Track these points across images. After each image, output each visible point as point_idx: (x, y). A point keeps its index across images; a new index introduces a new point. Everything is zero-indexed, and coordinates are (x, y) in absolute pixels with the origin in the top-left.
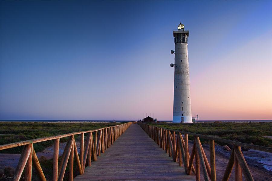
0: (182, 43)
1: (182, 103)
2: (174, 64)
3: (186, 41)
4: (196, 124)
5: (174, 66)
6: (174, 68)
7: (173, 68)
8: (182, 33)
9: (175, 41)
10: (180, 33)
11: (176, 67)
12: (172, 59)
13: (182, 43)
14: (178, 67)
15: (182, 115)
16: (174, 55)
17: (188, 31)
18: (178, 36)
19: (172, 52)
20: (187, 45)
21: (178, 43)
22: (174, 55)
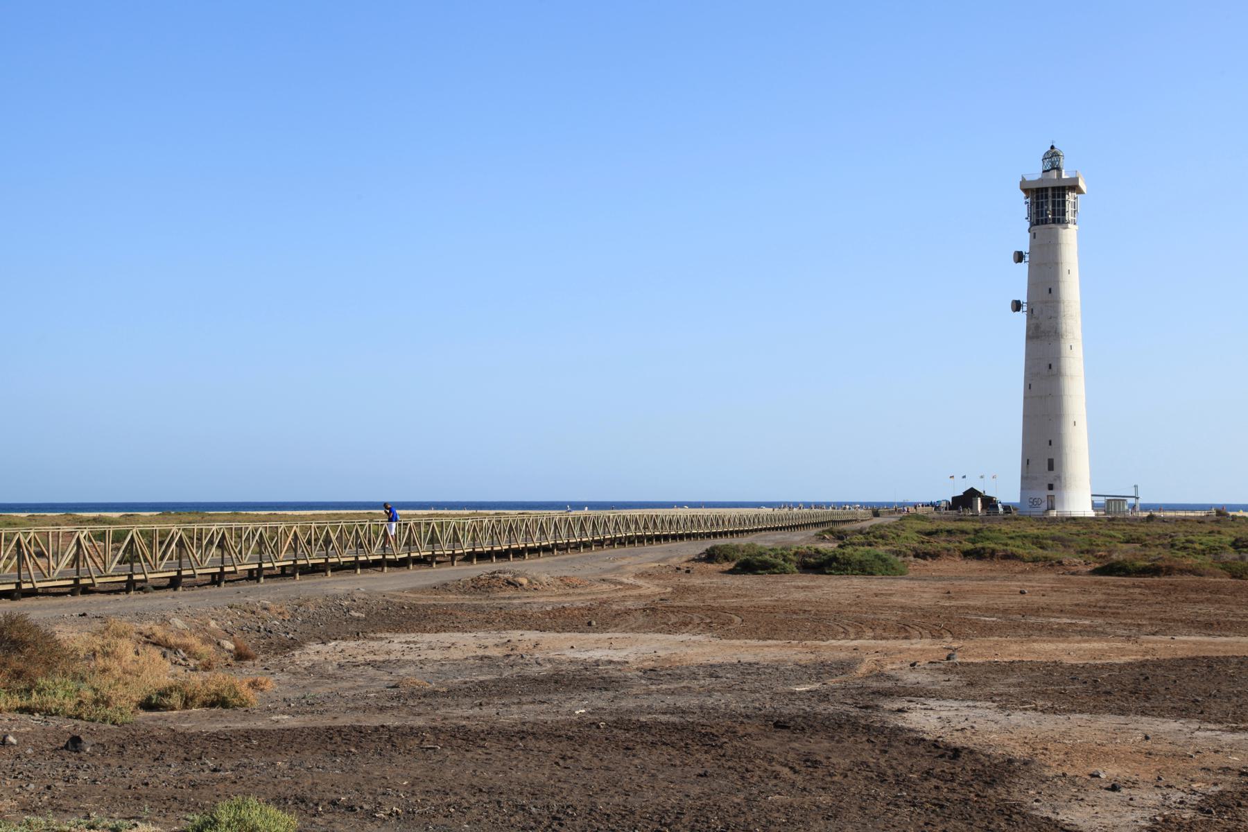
0: (1054, 222)
2: (1023, 299)
3: (1069, 216)
4: (1113, 515)
5: (1025, 308)
6: (1026, 265)
8: (1054, 189)
9: (1030, 215)
10: (1046, 189)
11: (1031, 312)
12: (1018, 281)
13: (1053, 226)
14: (946, 653)
15: (1051, 487)
16: (1024, 267)
17: (1076, 179)
20: (1076, 227)
21: (1038, 224)
22: (1024, 267)
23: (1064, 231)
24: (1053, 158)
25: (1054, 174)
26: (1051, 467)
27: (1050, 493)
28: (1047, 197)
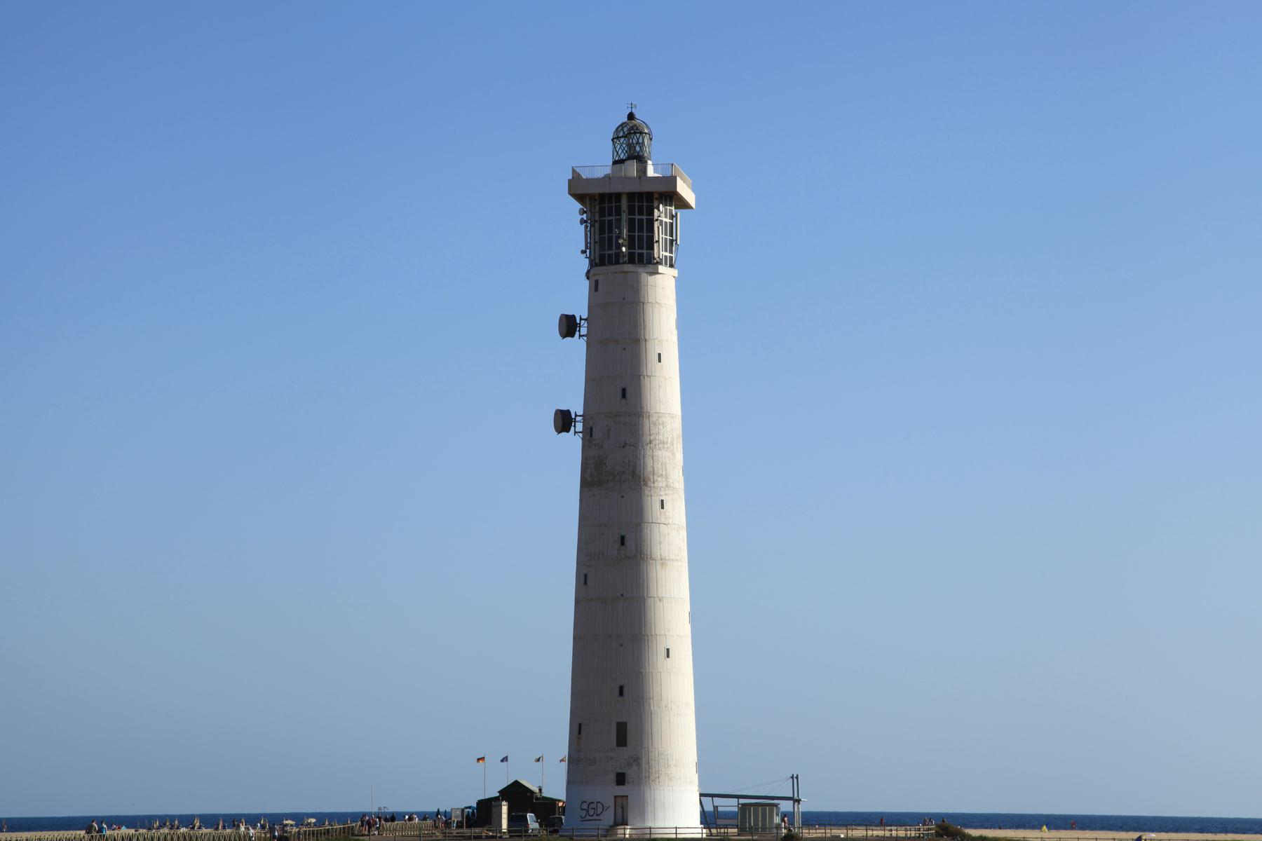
1: (621, 693)
2: (576, 407)
3: (660, 252)
5: (579, 427)
7: (572, 443)
8: (631, 196)
12: (566, 375)
14: (597, 435)
15: (621, 779)
16: (577, 346)
18: (602, 214)
19: (564, 421)
23: (651, 279)
24: (630, 137)
25: (632, 168)
26: (622, 740)
27: (620, 790)
28: (618, 212)
